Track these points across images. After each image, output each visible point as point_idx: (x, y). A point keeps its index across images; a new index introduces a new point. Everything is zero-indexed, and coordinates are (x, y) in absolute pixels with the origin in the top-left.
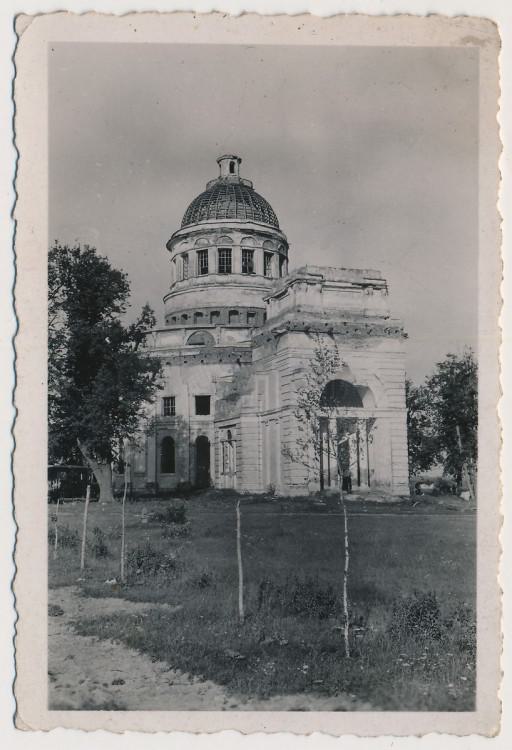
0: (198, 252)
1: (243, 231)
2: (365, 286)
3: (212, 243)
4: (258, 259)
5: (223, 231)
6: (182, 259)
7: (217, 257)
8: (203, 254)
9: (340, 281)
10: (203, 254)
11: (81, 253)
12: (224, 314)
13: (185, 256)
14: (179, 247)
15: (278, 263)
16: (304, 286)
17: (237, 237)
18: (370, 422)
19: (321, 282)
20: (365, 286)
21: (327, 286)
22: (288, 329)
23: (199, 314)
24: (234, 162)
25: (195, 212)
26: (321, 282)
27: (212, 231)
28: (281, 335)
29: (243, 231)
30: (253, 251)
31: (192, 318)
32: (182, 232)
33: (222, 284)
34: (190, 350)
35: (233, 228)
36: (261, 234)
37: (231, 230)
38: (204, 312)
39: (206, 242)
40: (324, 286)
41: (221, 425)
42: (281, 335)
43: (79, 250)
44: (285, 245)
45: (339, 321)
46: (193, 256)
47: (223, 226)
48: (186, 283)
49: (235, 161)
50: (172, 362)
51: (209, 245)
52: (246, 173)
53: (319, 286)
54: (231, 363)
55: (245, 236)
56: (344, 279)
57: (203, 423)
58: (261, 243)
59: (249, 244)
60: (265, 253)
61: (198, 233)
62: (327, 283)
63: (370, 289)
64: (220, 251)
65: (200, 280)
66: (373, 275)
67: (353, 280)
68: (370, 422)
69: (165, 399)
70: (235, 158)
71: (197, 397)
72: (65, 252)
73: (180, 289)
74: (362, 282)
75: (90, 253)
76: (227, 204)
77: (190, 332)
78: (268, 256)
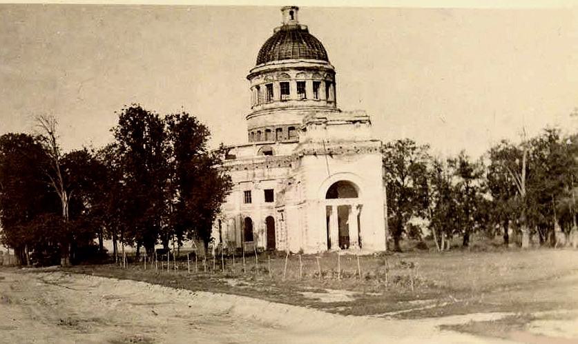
0: (266, 85)
1: (296, 69)
2: (354, 122)
3: (275, 78)
4: (309, 87)
5: (283, 69)
6: (256, 90)
7: (280, 89)
8: (270, 87)
9: (338, 120)
10: (270, 87)
11: (181, 117)
12: (285, 130)
13: (258, 87)
14: (256, 81)
15: (324, 88)
16: (314, 126)
17: (293, 73)
18: (359, 207)
19: (325, 122)
20: (354, 122)
21: (330, 125)
22: (304, 154)
23: (268, 131)
24: (293, 10)
25: (264, 56)
26: (325, 122)
27: (275, 70)
28: (301, 157)
29: (296, 69)
30: (305, 82)
31: (264, 134)
32: (255, 71)
33: (283, 109)
34: (259, 159)
35: (293, 65)
36: (309, 69)
37: (288, 69)
38: (271, 129)
39: (271, 78)
40: (328, 125)
41: (278, 209)
42: (301, 157)
43: (179, 115)
44: (331, 72)
45: (337, 146)
46: (263, 88)
47: (283, 66)
48: (259, 108)
49: (294, 10)
50: (248, 168)
51: (273, 80)
52: (303, 20)
53: (324, 125)
54: (286, 167)
55: (299, 72)
56: (339, 118)
57: (269, 207)
58: (311, 75)
59: (302, 78)
60: (314, 83)
61: (265, 72)
62: (328, 123)
63: (358, 123)
64: (281, 84)
65: (268, 106)
66: (361, 114)
67: (347, 119)
68: (359, 207)
69: (245, 192)
70: (293, 7)
71: (265, 191)
72: (171, 117)
73: (256, 112)
74: (353, 119)
75: (186, 116)
76: (288, 47)
77: (260, 147)
78: (316, 86)
